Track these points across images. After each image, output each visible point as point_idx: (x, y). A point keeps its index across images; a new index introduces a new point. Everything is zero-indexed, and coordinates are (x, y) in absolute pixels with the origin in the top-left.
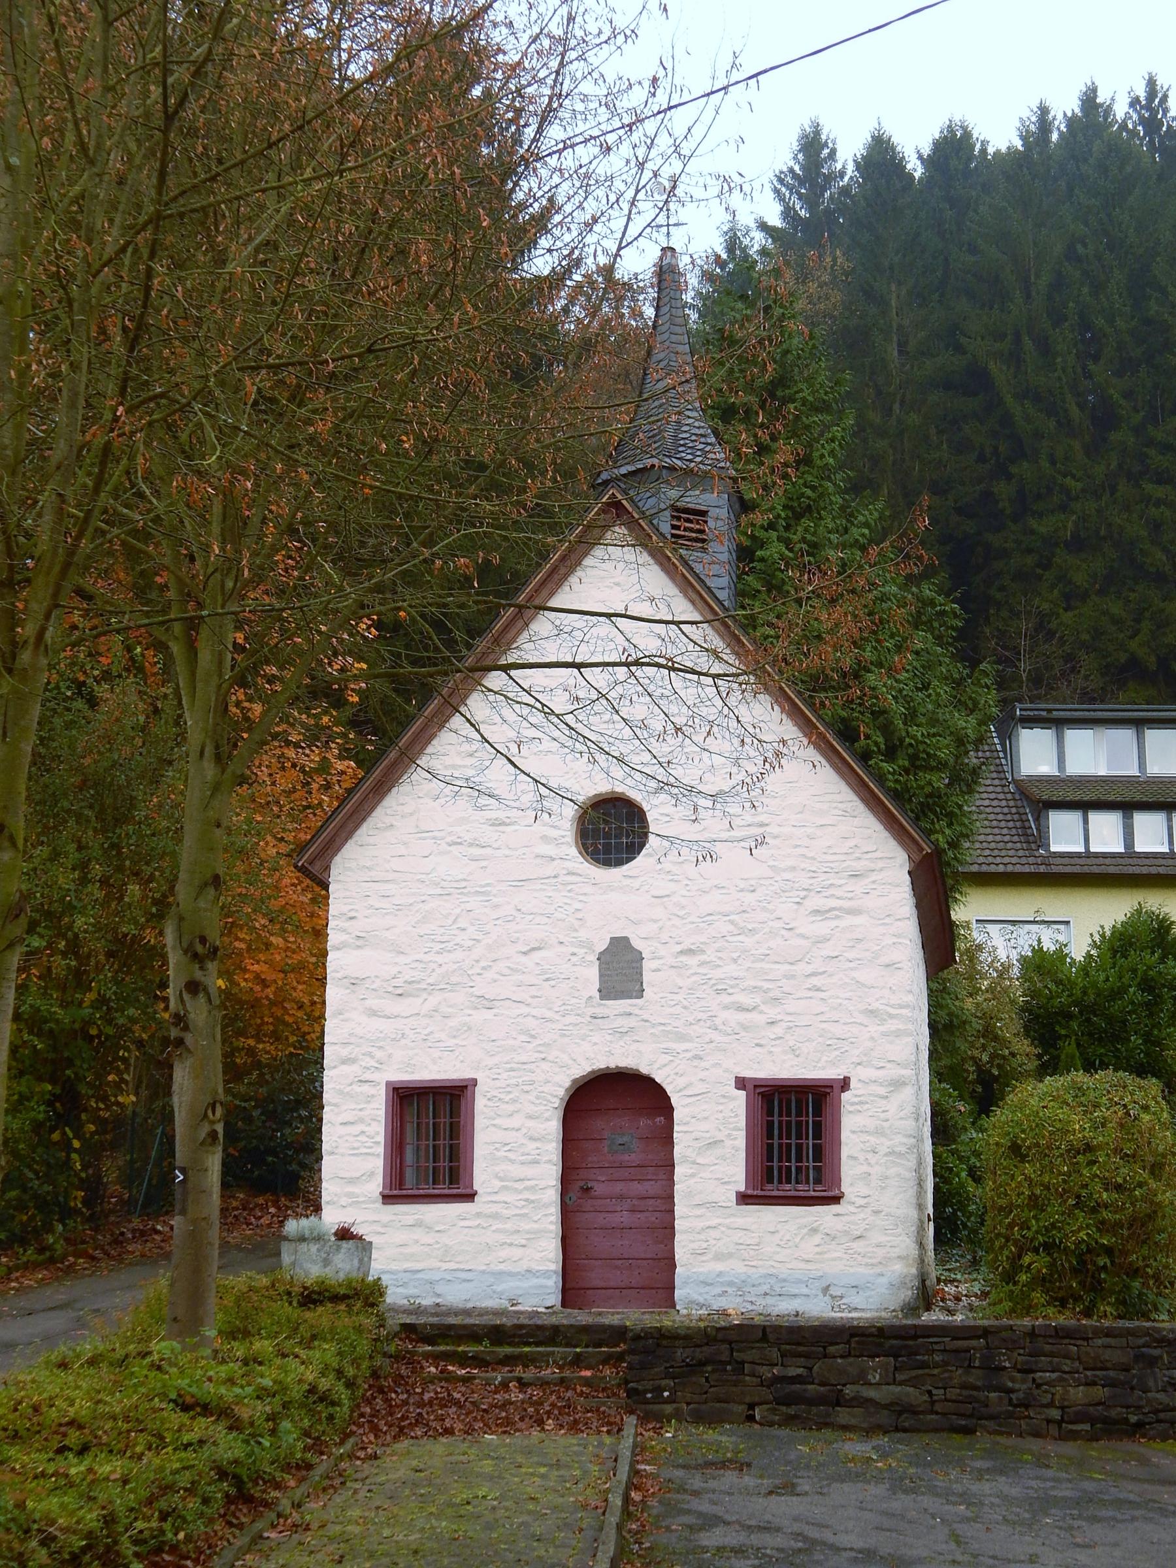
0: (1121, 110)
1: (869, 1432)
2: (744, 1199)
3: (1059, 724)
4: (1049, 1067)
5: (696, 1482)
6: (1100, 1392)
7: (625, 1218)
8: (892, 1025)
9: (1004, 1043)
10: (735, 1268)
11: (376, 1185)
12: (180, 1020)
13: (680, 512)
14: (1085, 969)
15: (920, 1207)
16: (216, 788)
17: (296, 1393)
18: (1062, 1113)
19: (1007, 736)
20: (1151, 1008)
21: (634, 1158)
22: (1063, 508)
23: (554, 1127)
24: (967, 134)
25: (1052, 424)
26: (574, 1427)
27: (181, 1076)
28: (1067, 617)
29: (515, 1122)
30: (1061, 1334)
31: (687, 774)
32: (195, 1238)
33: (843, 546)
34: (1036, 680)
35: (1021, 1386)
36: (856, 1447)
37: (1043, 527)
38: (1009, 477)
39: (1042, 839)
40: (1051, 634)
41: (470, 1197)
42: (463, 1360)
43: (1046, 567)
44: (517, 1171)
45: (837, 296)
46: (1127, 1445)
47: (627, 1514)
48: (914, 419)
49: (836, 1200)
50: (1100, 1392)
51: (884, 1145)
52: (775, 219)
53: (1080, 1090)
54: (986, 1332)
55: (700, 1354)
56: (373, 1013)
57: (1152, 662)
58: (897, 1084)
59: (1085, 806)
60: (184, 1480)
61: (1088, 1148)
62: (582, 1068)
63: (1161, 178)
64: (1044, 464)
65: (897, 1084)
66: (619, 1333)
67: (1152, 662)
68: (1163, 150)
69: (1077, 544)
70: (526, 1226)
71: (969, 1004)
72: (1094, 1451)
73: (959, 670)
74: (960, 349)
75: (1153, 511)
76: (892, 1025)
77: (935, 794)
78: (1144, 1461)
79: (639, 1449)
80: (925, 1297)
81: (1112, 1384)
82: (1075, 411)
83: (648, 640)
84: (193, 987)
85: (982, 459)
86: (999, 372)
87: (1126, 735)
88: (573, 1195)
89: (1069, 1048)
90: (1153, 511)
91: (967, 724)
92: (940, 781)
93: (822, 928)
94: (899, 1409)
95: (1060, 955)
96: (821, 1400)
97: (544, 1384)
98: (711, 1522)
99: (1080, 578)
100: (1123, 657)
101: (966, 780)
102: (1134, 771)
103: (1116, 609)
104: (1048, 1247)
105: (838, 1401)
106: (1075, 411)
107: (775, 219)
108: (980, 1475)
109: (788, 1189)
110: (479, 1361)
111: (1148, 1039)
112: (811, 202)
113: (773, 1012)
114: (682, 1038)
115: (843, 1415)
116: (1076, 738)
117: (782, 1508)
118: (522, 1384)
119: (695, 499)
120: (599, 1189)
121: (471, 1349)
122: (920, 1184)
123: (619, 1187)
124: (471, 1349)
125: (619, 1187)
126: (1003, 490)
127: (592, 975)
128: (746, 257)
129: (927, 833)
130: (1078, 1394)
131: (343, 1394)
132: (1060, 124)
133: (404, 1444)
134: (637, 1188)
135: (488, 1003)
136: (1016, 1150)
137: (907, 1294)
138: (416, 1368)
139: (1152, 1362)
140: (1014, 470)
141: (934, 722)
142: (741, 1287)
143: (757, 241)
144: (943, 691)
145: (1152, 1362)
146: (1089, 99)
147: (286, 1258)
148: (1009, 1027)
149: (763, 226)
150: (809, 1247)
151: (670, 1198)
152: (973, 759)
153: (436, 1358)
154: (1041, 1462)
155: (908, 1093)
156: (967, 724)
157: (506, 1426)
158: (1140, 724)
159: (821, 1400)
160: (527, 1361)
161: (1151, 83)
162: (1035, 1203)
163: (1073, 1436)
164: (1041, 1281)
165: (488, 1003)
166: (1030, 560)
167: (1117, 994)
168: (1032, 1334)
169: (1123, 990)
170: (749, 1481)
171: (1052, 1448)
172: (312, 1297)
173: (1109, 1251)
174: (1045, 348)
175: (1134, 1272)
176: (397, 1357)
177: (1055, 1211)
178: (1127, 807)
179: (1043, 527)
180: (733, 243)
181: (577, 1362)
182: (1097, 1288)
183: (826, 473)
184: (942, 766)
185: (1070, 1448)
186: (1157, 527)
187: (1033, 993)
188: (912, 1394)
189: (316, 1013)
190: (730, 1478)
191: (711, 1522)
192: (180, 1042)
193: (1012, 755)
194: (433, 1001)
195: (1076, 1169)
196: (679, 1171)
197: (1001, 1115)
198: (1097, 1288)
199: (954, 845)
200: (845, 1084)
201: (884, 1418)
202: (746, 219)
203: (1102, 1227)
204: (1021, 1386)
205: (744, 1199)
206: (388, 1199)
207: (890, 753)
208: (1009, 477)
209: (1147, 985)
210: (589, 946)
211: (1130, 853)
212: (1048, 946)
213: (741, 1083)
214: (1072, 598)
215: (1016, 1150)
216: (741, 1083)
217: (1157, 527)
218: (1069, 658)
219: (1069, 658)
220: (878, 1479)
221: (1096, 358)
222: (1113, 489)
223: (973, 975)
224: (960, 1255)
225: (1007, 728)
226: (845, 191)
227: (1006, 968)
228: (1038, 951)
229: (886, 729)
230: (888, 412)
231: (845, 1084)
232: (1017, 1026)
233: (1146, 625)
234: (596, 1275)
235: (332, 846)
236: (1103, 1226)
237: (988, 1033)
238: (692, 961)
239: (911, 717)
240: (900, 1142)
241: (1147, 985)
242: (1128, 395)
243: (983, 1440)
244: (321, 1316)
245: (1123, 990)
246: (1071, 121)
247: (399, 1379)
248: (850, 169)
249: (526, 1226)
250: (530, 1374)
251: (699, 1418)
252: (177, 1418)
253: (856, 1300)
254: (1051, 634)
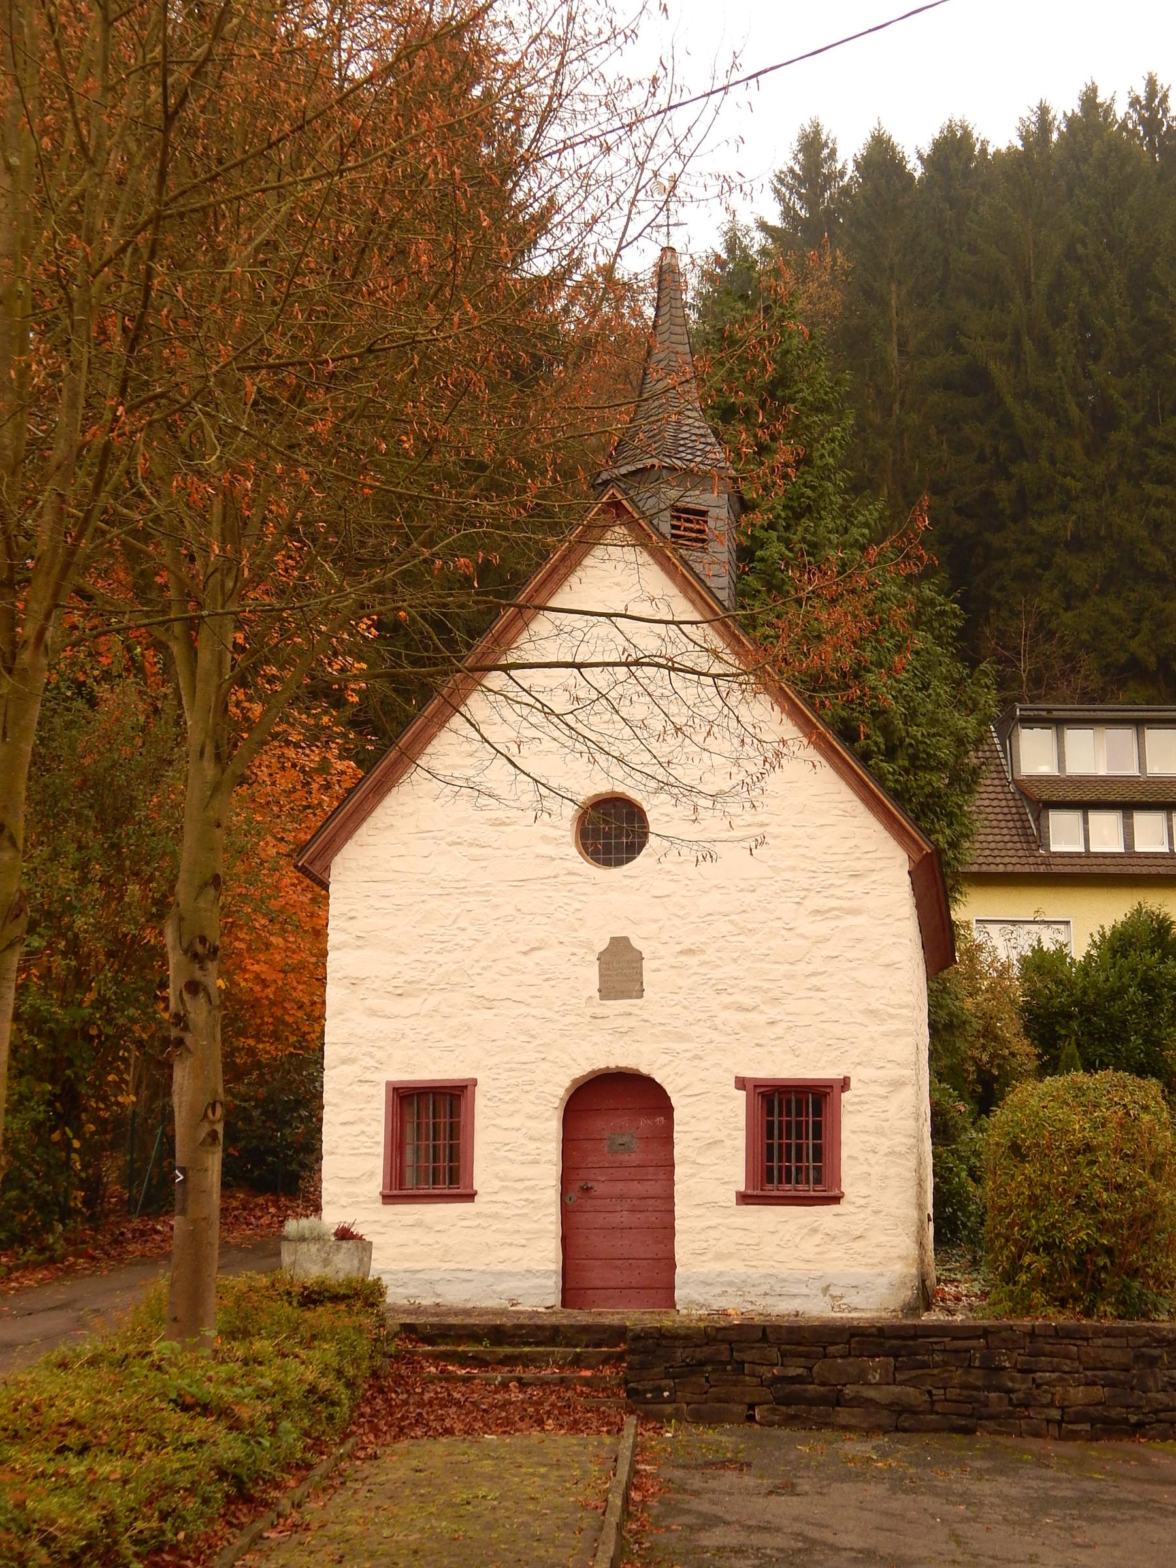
0: (1121, 110)
1: (868, 1432)
2: (744, 1199)
3: (1059, 724)
4: (1049, 1067)
5: (696, 1482)
6: (1100, 1392)
7: (625, 1218)
8: (893, 1025)
9: (1005, 1043)
10: (735, 1268)
11: (376, 1185)
12: (180, 1020)
13: (680, 512)
14: (1085, 969)
15: (920, 1207)
16: (216, 788)
17: (296, 1392)
18: (1065, 1111)
19: (1007, 735)
20: (1151, 1007)
21: (634, 1158)
22: (1064, 508)
23: (554, 1127)
24: (967, 134)
25: (1052, 424)
26: (574, 1427)
27: (181, 1076)
28: (1067, 617)
29: (515, 1122)
30: (1061, 1334)
31: (686, 774)
32: (195, 1238)
33: (843, 546)
34: (1036, 680)
35: (1021, 1386)
36: (856, 1447)
37: (1043, 527)
38: (1009, 477)
39: (1042, 839)
40: (1051, 634)
41: (470, 1197)
42: (464, 1360)
43: (1046, 567)
44: (517, 1171)
45: (837, 297)
46: (1127, 1445)
47: (627, 1514)
48: (914, 419)
49: (836, 1200)
50: (1100, 1392)
51: (884, 1144)
52: (775, 219)
53: (1080, 1090)
54: (986, 1332)
55: (701, 1354)
56: (373, 1013)
57: (1152, 662)
58: (897, 1084)
59: (1085, 807)
60: (184, 1480)
61: (1088, 1148)
62: (582, 1068)
63: (1160, 178)
64: (1045, 464)
65: (897, 1084)
66: (619, 1333)
67: (1152, 662)
68: (1163, 150)
69: (1077, 545)
70: (526, 1226)
71: (969, 1003)
72: (1094, 1451)
73: (960, 670)
74: (959, 349)
75: (1153, 512)
76: (893, 1025)
77: (936, 794)
78: (1144, 1461)
79: (639, 1449)
80: (925, 1297)
81: (1111, 1383)
82: (1074, 411)
83: (648, 640)
84: (194, 987)
85: (982, 459)
86: (999, 372)
87: (1126, 735)
88: (574, 1195)
89: (1069, 1048)
90: (1153, 512)
91: (967, 724)
92: (940, 781)
93: (822, 928)
94: (899, 1409)
95: (1060, 955)
96: (821, 1400)
97: (543, 1383)
98: (711, 1522)
99: (1080, 579)
100: (1123, 658)
101: (965, 780)
102: (1134, 771)
103: (1117, 609)
104: (1048, 1247)
105: (838, 1401)
106: (1074, 411)
107: (775, 219)
108: (980, 1475)
109: (788, 1189)
110: (479, 1361)
111: (1148, 1039)
112: (811, 202)
113: (773, 1012)
114: (682, 1038)
115: (844, 1415)
116: (1076, 738)
117: (781, 1508)
118: (522, 1384)
119: (695, 499)
120: (599, 1189)
121: (471, 1349)
122: (920, 1184)
123: (619, 1187)
124: (471, 1349)
125: (619, 1187)
126: (1004, 490)
127: (591, 975)
128: (746, 257)
129: (927, 833)
130: (1078, 1395)
131: (342, 1393)
132: (1060, 124)
133: (404, 1444)
134: (637, 1188)
135: (488, 1003)
136: (1016, 1150)
137: (907, 1294)
138: (416, 1368)
139: (1153, 1362)
140: (1013, 469)
141: (933, 722)
142: (741, 1287)
143: (757, 241)
144: (943, 691)
145: (1153, 1362)
146: (1089, 99)
147: (286, 1258)
148: (1009, 1027)
149: (763, 226)
150: (809, 1247)
151: (670, 1198)
152: (973, 759)
153: (436, 1358)
154: (1041, 1461)
155: (908, 1093)
156: (967, 724)
157: (507, 1426)
158: (1140, 724)
159: (821, 1400)
160: (527, 1361)
161: (1151, 83)
162: (1035, 1203)
163: (1073, 1436)
164: (1042, 1281)
165: (488, 1003)
166: (1030, 560)
167: (1117, 994)
168: (1032, 1334)
169: (1123, 990)
170: (749, 1481)
171: (1051, 1447)
172: (312, 1297)
173: (1109, 1251)
174: (1045, 348)
175: (1134, 1273)
176: (397, 1357)
177: (1054, 1212)
178: (1127, 807)
179: (1043, 527)
180: (733, 243)
181: (577, 1362)
182: (1097, 1288)
183: (826, 473)
184: (942, 766)
185: (1070, 1448)
186: (1157, 527)
187: (1033, 993)
188: (911, 1394)
189: (316, 1014)
190: (730, 1478)
191: (711, 1522)
192: (180, 1042)
193: (1011, 754)
194: (433, 1001)
195: (1075, 1169)
196: (679, 1171)
197: (1001, 1115)
198: (1097, 1288)
199: (954, 845)
200: (845, 1084)
201: (884, 1418)
202: (746, 219)
203: (1102, 1227)
204: (1021, 1386)
205: (744, 1199)
206: (388, 1199)
207: (890, 753)
208: (1009, 477)
209: (1147, 985)
210: (589, 946)
211: (1130, 853)
212: (1048, 946)
213: (741, 1083)
214: (1073, 597)
215: (1016, 1150)
216: (741, 1083)
217: (1157, 527)
218: (1069, 658)
219: (1069, 658)
220: (878, 1479)
221: (1096, 358)
222: (1113, 489)
223: (973, 975)
224: (961, 1255)
225: (1007, 727)
226: (845, 191)
227: (1006, 968)
228: (1038, 951)
229: (886, 729)
230: (888, 411)
231: (845, 1084)
232: (1017, 1025)
233: (1146, 625)
234: (596, 1275)
235: (332, 846)
236: (1103, 1226)
237: (988, 1033)
238: (692, 961)
239: (911, 716)
240: (901, 1142)
241: (1147, 985)
242: (1128, 395)
243: (983, 1439)
244: (321, 1316)
245: (1123, 990)
246: (1071, 121)
247: (399, 1379)
248: (850, 169)
249: (526, 1226)
250: (530, 1374)
251: (699, 1418)
252: (177, 1418)
253: (854, 1299)
254: (1051, 634)
